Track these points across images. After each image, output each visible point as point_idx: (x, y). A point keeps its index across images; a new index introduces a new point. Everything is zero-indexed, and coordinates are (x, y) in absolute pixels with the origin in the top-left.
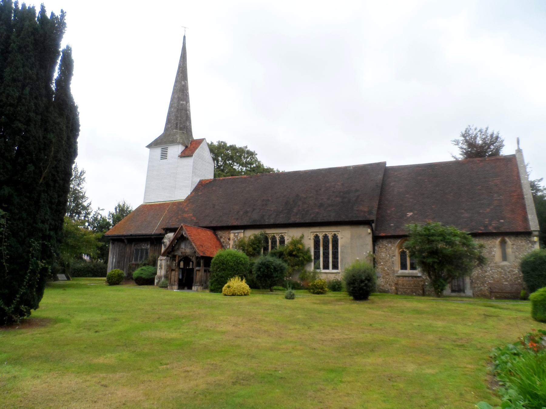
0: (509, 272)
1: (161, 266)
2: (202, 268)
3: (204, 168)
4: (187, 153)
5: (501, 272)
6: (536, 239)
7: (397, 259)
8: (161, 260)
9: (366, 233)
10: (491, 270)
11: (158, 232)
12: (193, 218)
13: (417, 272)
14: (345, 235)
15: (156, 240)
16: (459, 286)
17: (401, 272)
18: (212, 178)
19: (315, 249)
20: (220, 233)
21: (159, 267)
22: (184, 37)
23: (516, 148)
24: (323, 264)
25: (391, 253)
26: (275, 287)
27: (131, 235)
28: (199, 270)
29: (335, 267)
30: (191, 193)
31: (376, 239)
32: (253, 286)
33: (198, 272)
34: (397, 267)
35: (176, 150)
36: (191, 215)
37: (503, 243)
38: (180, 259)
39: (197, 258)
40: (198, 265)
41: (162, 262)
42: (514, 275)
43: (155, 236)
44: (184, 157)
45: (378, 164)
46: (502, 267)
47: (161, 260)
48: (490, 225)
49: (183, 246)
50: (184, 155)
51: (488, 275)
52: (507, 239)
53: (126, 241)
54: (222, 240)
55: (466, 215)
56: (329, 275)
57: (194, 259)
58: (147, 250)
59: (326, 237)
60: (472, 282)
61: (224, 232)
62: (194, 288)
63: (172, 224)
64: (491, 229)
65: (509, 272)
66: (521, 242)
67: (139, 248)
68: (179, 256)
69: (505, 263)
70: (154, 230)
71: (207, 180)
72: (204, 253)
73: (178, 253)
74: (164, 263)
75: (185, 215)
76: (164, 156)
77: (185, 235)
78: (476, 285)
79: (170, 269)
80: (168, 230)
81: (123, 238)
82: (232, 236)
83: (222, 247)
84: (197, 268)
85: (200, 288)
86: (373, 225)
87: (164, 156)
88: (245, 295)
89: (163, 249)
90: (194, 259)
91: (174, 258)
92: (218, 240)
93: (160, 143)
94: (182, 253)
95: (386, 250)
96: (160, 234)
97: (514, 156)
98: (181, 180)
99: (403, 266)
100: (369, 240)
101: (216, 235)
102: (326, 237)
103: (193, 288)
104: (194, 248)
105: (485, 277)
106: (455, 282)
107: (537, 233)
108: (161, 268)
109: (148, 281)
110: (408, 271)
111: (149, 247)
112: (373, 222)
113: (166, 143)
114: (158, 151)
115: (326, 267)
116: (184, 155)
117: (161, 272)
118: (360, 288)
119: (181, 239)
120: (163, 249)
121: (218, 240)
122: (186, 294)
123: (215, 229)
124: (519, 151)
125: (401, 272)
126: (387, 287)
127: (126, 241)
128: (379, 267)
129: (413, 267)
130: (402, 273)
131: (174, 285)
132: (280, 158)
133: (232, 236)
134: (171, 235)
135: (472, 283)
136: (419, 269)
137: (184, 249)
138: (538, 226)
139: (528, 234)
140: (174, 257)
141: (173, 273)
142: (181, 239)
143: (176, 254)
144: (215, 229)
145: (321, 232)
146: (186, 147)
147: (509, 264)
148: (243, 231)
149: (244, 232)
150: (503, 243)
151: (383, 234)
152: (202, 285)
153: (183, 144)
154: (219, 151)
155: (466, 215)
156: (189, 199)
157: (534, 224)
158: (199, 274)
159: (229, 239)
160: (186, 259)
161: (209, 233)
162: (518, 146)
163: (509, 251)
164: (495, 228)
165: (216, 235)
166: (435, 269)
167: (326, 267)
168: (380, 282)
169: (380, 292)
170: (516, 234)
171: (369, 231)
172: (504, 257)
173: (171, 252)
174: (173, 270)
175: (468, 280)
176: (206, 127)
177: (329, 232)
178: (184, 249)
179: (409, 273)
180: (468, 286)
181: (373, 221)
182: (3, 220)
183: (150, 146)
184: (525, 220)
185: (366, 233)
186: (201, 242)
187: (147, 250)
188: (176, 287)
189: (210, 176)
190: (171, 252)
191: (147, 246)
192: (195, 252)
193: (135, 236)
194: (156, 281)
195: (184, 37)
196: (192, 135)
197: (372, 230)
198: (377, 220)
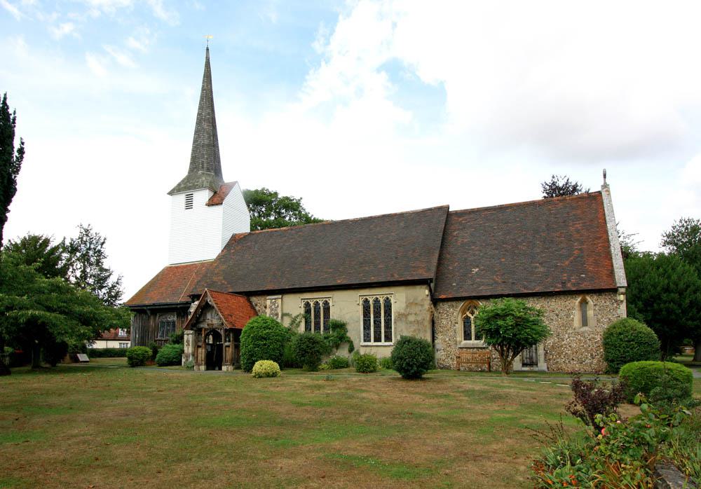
0: (590, 340)
1: (188, 341)
3: (236, 218)
4: (216, 200)
5: (580, 340)
6: (622, 297)
7: (460, 327)
8: (188, 334)
9: (423, 292)
10: (569, 337)
11: (184, 300)
12: (223, 282)
13: (481, 343)
14: (399, 299)
15: (182, 310)
16: (531, 358)
17: (465, 343)
18: (247, 230)
19: (364, 317)
20: (254, 300)
21: (185, 343)
22: (208, 49)
23: (602, 183)
24: (375, 335)
25: (452, 317)
27: (154, 305)
28: (229, 346)
29: (388, 338)
30: (222, 251)
31: (435, 301)
33: (227, 349)
34: (460, 336)
35: (202, 196)
36: (221, 278)
37: (584, 303)
38: (206, 332)
39: (226, 330)
42: (596, 343)
43: (181, 306)
44: (213, 205)
45: (440, 208)
46: (582, 334)
47: (188, 334)
48: (569, 281)
49: (209, 316)
50: (211, 203)
51: (565, 344)
52: (588, 298)
53: (148, 312)
54: (257, 308)
55: (542, 270)
56: (368, 349)
57: (222, 333)
58: (174, 322)
59: (377, 301)
60: (547, 353)
61: (259, 298)
62: (224, 368)
64: (570, 286)
65: (590, 340)
66: (604, 301)
67: (164, 320)
68: (205, 329)
69: (585, 328)
70: (181, 298)
71: (242, 234)
72: (233, 325)
75: (215, 279)
76: (189, 205)
77: (210, 303)
78: (551, 357)
80: (195, 297)
81: (145, 308)
82: (268, 302)
83: (256, 313)
84: (227, 344)
86: (432, 285)
87: (189, 205)
88: (272, 376)
93: (185, 187)
94: (208, 325)
95: (448, 316)
96: (187, 303)
97: (600, 193)
98: (203, 235)
99: (467, 336)
101: (250, 303)
102: (377, 301)
103: (223, 367)
104: (220, 319)
105: (562, 346)
106: (525, 353)
107: (623, 290)
108: (188, 345)
109: (175, 361)
110: (473, 342)
112: (431, 282)
113: (189, 188)
114: (181, 198)
115: (378, 339)
116: (211, 203)
117: (188, 349)
118: (414, 363)
119: (205, 308)
123: (249, 295)
124: (605, 186)
125: (465, 343)
126: (449, 362)
127: (148, 312)
128: (440, 337)
129: (478, 338)
130: (466, 344)
131: (201, 365)
132: (326, 206)
133: (268, 302)
135: (546, 354)
136: (676, 298)
137: (212, 320)
138: (625, 281)
139: (615, 291)
140: (200, 330)
141: (200, 350)
143: (202, 326)
145: (372, 294)
146: (215, 193)
147: (590, 329)
148: (280, 296)
149: (282, 298)
150: (584, 303)
152: (233, 365)
153: (211, 188)
154: (257, 200)
155: (542, 270)
156: (219, 258)
157: (621, 279)
159: (266, 307)
161: (242, 300)
162: (605, 181)
163: (590, 313)
164: (574, 285)
166: (597, 436)
167: (378, 339)
168: (440, 355)
169: (442, 368)
170: (599, 292)
171: (427, 292)
172: (585, 322)
173: (195, 325)
174: (199, 347)
175: (541, 351)
176: (243, 168)
177: (381, 294)
178: (212, 320)
179: (473, 344)
180: (541, 358)
181: (431, 280)
183: (171, 193)
184: (611, 273)
187: (174, 322)
188: (203, 368)
189: (245, 228)
191: (172, 318)
192: (223, 324)
193: (160, 305)
194: (183, 360)
195: (208, 49)
196: (222, 177)
197: (430, 291)
198: (436, 279)
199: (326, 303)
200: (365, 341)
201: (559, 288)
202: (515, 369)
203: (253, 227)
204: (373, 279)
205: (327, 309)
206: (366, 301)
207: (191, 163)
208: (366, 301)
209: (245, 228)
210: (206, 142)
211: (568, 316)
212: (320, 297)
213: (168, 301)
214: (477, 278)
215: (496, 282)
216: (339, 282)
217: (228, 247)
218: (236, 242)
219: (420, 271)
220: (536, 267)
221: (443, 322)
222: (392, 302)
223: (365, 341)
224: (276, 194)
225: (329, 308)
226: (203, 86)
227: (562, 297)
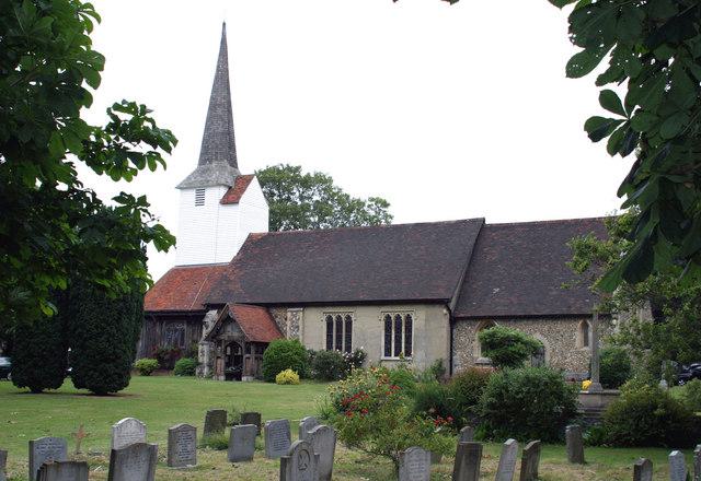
1: (202, 352)
2: (253, 355)
3: (253, 214)
9: (441, 314)
14: (419, 317)
15: (196, 318)
20: (274, 311)
22: (224, 24)
26: (46, 390)
27: (161, 312)
31: (454, 321)
32: (303, 376)
37: (585, 326)
40: (248, 351)
41: (204, 350)
45: (474, 221)
49: (229, 328)
50: (226, 201)
54: (277, 320)
57: (243, 345)
62: (244, 379)
63: (215, 299)
70: (192, 305)
71: (260, 235)
73: (224, 337)
74: (206, 348)
76: (200, 201)
79: (213, 355)
82: (289, 314)
85: (250, 378)
86: (452, 305)
87: (200, 201)
89: (205, 332)
90: (243, 345)
91: (219, 343)
92: (273, 319)
96: (199, 311)
100: (445, 322)
101: (270, 314)
102: (398, 317)
109: (189, 372)
111: (185, 327)
114: (192, 194)
116: (226, 201)
117: (203, 359)
119: (226, 320)
120: (205, 332)
121: (273, 319)
122: (234, 384)
123: (268, 306)
133: (289, 314)
134: (213, 315)
137: (231, 333)
141: (219, 361)
142: (226, 320)
144: (268, 306)
146: (230, 188)
150: (585, 326)
151: (462, 315)
154: (277, 181)
158: (249, 362)
160: (234, 345)
161: (261, 311)
165: (270, 314)
171: (445, 311)
173: (214, 337)
174: (218, 357)
177: (402, 311)
178: (231, 333)
182: (488, 464)
183: (179, 188)
185: (441, 314)
186: (251, 323)
189: (263, 227)
190: (214, 337)
195: (224, 24)
199: (349, 318)
200: (386, 355)
201: (564, 311)
202: (325, 348)
203: (273, 224)
204: (394, 297)
205: (349, 324)
206: (388, 317)
207: (202, 154)
208: (388, 317)
209: (263, 227)
210: (220, 130)
211: (571, 337)
212: (342, 312)
213: (178, 308)
214: (498, 298)
215: (512, 302)
216: (361, 298)
217: (244, 249)
218: (253, 244)
219: (442, 291)
220: (551, 290)
221: (461, 338)
222: (413, 318)
223: (386, 355)
224: (298, 169)
225: (351, 322)
226: (218, 67)
227: (530, 322)
